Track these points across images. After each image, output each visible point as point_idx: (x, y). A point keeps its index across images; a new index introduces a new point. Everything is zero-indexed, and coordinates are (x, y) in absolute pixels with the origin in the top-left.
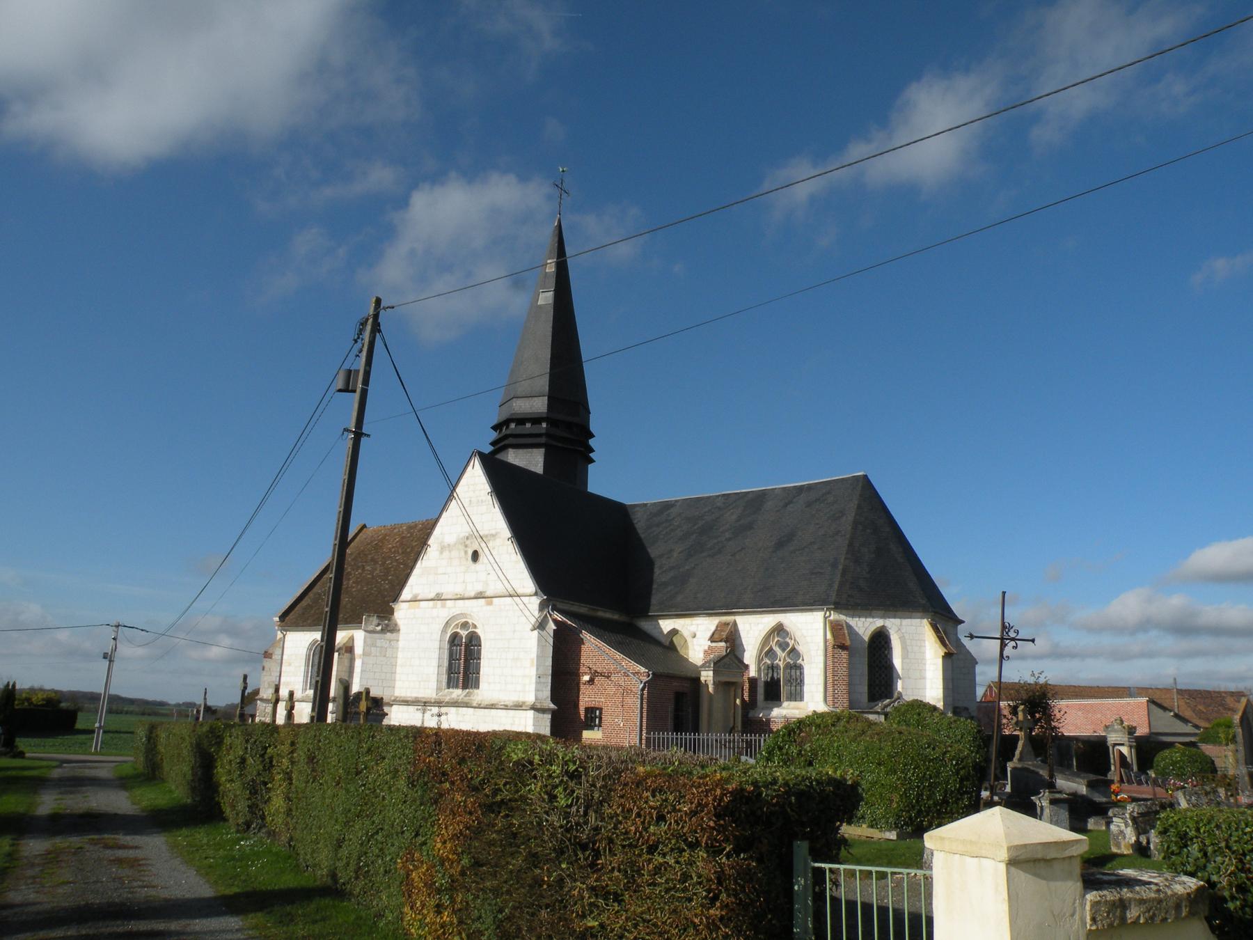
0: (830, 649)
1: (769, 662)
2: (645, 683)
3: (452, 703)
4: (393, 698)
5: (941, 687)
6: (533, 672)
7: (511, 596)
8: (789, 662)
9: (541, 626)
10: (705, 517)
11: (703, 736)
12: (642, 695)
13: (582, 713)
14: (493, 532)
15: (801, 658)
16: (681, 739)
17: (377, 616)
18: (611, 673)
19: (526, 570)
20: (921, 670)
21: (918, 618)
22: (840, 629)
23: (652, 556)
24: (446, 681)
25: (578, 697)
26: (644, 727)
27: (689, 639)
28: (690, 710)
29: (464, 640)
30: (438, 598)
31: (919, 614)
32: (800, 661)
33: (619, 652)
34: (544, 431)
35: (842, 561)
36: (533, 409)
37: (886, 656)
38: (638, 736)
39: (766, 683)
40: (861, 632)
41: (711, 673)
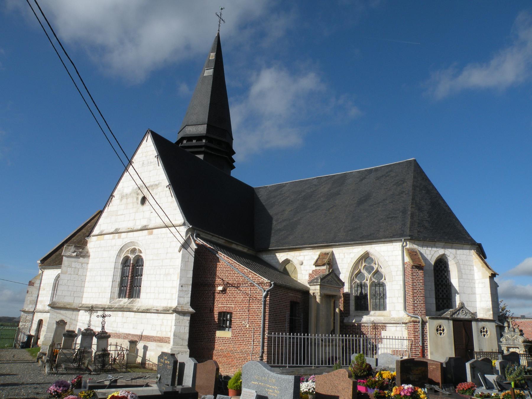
0: (409, 269)
1: (358, 282)
2: (268, 292)
3: (120, 308)
4: (80, 305)
5: (490, 300)
6: (176, 283)
7: (167, 227)
8: (374, 281)
9: (185, 245)
10: (306, 191)
11: (311, 336)
12: (265, 301)
13: (216, 316)
14: (157, 183)
15: (383, 278)
16: (297, 338)
17: (74, 246)
18: (240, 284)
19: (167, 180)
20: (472, 287)
21: (467, 249)
22: (416, 255)
23: (271, 214)
24: (118, 292)
25: (214, 304)
26: (266, 328)
27: (298, 266)
28: (302, 316)
29: (132, 262)
30: (117, 232)
31: (469, 246)
32: (382, 280)
33: (246, 267)
34: (204, 144)
35: (410, 208)
36: (198, 132)
37: (446, 277)
38: (261, 336)
39: (357, 298)
40: (429, 257)
41: (318, 287)
